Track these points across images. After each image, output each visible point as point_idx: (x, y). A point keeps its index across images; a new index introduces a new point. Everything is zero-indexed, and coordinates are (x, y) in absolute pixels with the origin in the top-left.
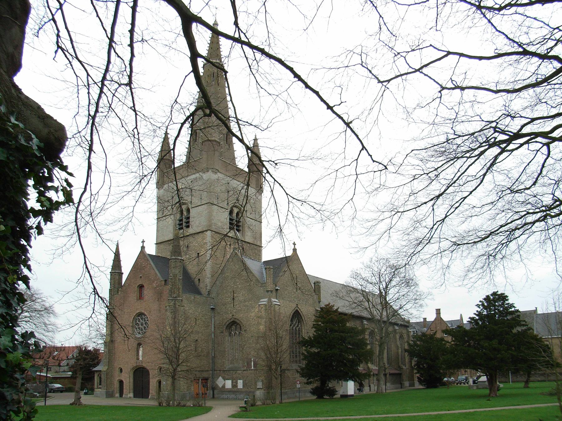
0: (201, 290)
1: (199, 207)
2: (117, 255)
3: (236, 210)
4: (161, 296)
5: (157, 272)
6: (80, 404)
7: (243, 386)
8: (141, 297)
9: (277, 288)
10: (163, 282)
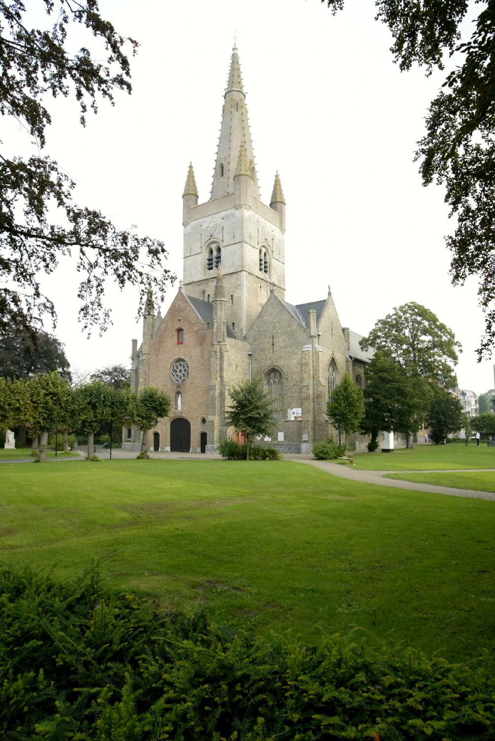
0: (236, 335)
1: (232, 246)
3: (264, 250)
4: (204, 341)
5: (198, 314)
6: (148, 457)
7: (285, 438)
9: (319, 333)
10: (206, 326)
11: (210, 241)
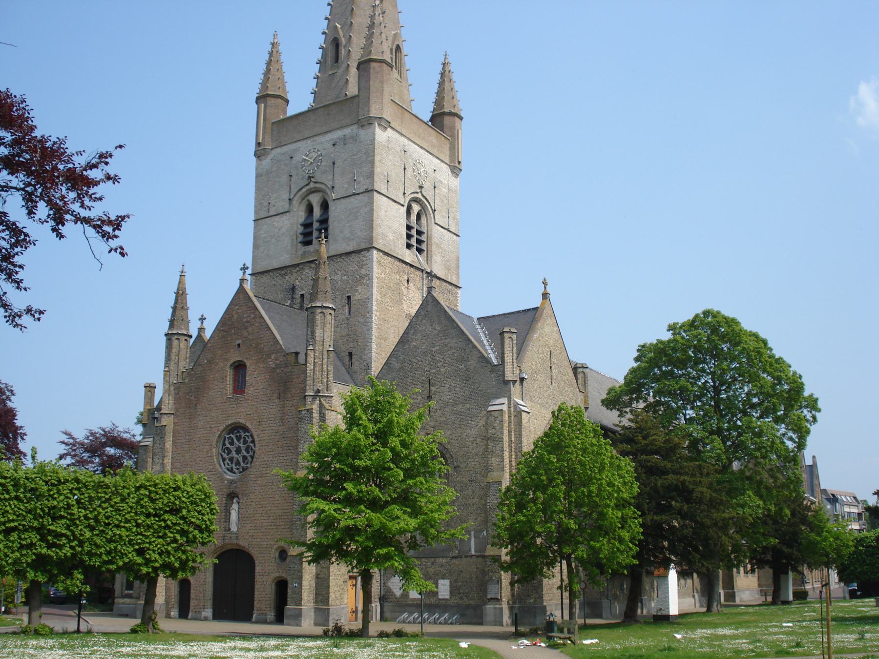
1: (352, 199)
2: (180, 295)
3: (416, 208)
7: (451, 593)
8: (239, 387)
11: (308, 187)
